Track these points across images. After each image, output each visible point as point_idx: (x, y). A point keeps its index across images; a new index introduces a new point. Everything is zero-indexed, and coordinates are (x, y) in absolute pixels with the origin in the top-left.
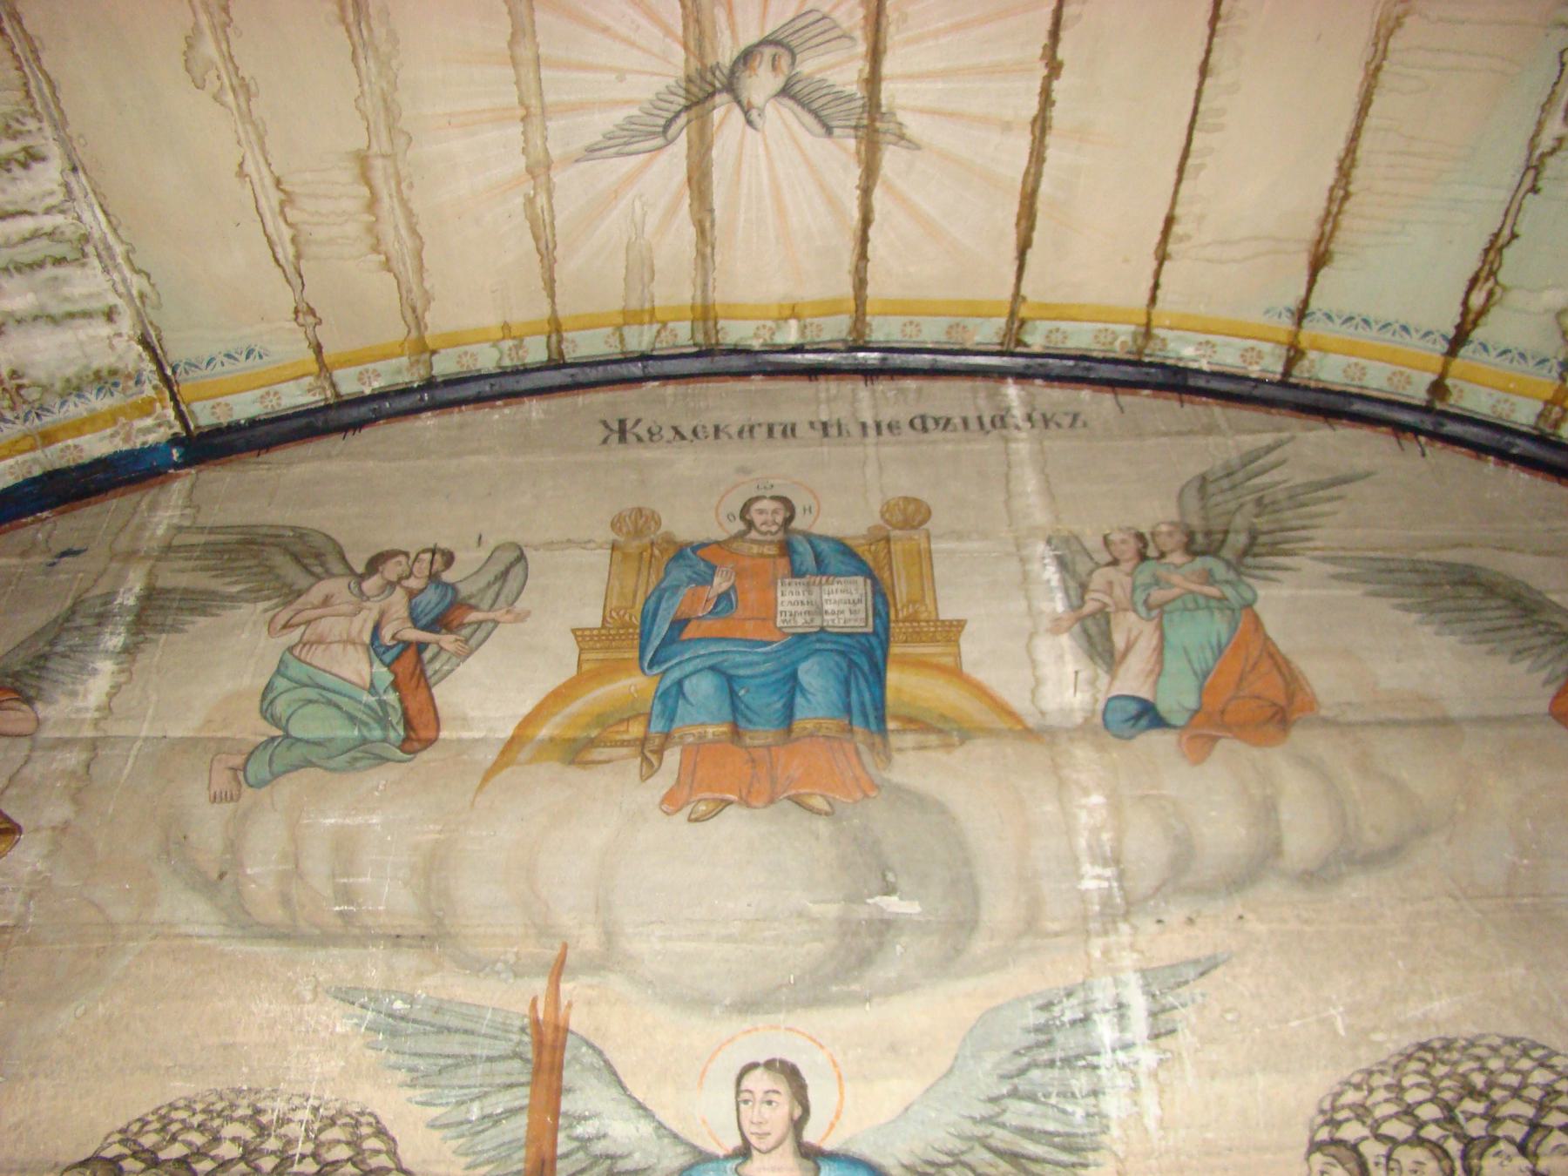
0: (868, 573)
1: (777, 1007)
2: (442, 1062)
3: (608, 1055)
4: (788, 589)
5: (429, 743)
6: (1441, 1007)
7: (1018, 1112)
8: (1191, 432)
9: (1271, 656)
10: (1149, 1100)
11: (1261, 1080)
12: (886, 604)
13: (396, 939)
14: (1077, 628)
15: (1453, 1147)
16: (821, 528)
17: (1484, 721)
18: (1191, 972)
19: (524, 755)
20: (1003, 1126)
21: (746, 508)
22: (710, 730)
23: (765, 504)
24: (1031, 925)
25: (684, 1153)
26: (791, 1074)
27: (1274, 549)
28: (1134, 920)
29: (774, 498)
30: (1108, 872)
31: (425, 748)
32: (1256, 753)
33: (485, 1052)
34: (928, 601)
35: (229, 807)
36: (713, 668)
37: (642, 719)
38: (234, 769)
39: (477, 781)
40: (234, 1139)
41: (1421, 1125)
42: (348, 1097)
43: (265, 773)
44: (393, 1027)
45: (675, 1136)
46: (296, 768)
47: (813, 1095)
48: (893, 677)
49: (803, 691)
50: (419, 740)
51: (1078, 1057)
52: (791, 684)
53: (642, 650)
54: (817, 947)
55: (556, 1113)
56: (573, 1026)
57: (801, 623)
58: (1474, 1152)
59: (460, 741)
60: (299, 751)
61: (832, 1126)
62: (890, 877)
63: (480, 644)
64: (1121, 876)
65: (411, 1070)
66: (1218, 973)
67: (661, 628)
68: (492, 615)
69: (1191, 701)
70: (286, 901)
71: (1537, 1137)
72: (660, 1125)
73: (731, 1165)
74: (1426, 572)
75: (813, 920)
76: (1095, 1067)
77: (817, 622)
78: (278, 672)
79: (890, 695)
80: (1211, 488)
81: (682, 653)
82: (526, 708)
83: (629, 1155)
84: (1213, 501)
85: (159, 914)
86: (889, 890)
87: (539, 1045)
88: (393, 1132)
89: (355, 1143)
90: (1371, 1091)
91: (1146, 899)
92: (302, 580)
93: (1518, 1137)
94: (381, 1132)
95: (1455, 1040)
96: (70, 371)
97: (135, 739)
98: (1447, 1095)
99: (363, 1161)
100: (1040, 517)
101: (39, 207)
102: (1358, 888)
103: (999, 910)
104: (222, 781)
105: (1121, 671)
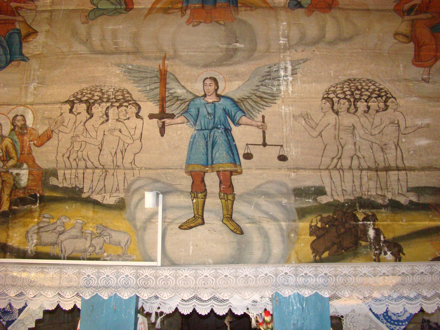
2: (140, 78)
3: (176, 76)
5: (131, 9)
6: (354, 72)
10: (290, 89)
11: (314, 84)
13: (128, 53)
15: (352, 100)
17: (378, 10)
19: (154, 11)
20: (259, 91)
22: (197, 6)
24: (268, 50)
28: (291, 50)
31: (130, 10)
32: (323, 15)
33: (150, 76)
35: (86, 25)
37: (181, 3)
38: (86, 16)
39: (143, 18)
40: (97, 96)
41: (346, 95)
42: (121, 86)
43: (94, 17)
44: (129, 71)
45: (191, 93)
46: (101, 15)
47: (219, 84)
50: (129, 8)
51: (276, 78)
55: (165, 88)
56: (168, 70)
58: (356, 101)
59: (139, 8)
60: (101, 12)
61: (223, 91)
64: (288, 41)
65: (134, 80)
66: (307, 62)
70: (102, 45)
71: (370, 99)
72: (187, 90)
75: (220, 48)
76: (279, 80)
83: (181, 96)
86: (237, 42)
88: (131, 93)
89: (123, 95)
90: (337, 88)
91: (294, 45)
93: (366, 99)
94: (128, 93)
97: (61, 10)
98: (353, 90)
99: (125, 99)
102: (341, 46)
103: (261, 47)
104: (84, 19)
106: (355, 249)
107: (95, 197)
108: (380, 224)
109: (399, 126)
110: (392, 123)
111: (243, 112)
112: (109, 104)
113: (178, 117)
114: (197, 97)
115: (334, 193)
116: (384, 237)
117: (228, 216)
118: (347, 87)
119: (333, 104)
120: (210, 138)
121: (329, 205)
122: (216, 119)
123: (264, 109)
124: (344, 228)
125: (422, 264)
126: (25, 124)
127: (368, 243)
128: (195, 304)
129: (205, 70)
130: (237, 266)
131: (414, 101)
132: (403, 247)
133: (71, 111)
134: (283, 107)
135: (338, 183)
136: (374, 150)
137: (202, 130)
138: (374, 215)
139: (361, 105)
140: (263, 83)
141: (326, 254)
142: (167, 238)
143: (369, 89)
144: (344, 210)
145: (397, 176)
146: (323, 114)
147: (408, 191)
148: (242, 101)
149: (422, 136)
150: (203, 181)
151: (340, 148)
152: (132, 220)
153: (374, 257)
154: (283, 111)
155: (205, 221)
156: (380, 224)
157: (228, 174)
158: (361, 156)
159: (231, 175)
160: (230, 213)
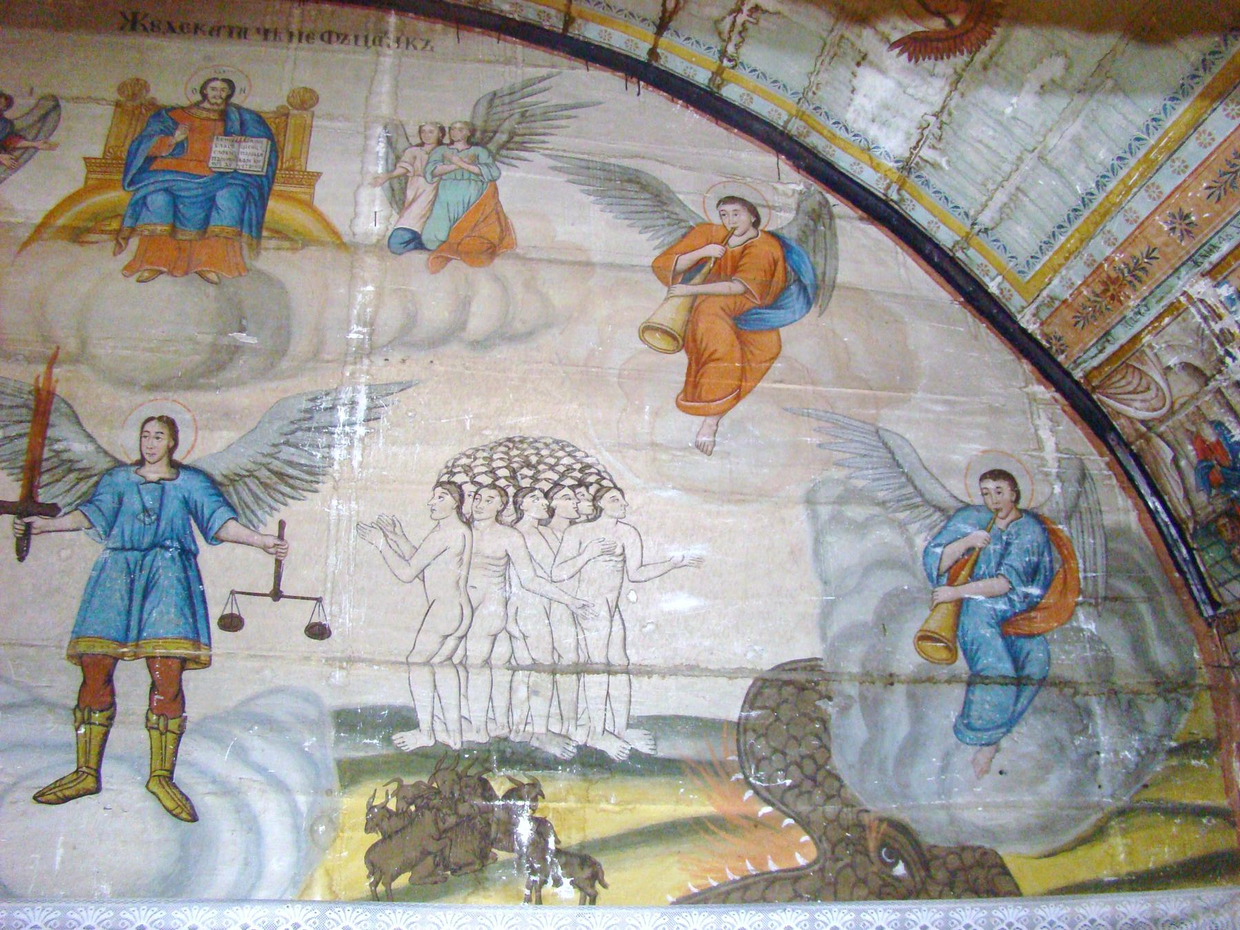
0: (270, 136)
1: (169, 389)
4: (219, 143)
7: (288, 453)
8: (498, 62)
9: (497, 213)
12: (277, 157)
14: (387, 184)
16: (246, 105)
21: (204, 87)
22: (159, 228)
23: (218, 84)
24: (316, 355)
25: (982, 670)
26: (171, 424)
27: (522, 147)
29: (224, 80)
30: (365, 330)
32: (470, 270)
33: (9, 404)
34: (303, 160)
39: (15, 248)
41: (498, 479)
47: (181, 436)
48: (272, 204)
49: (218, 209)
52: (210, 204)
53: (126, 173)
54: (197, 358)
55: (44, 438)
57: (223, 166)
59: (9, 223)
61: (189, 452)
62: (244, 322)
63: (26, 161)
64: (371, 334)
66: (410, 390)
67: (139, 162)
68: (35, 144)
69: (442, 236)
72: (99, 447)
73: (133, 469)
74: (609, 171)
77: (233, 166)
79: (268, 215)
80: (497, 102)
81: (148, 178)
82: (51, 206)
84: (494, 110)
86: (242, 330)
87: (38, 401)
90: (475, 459)
95: (525, 438)
98: (515, 466)
100: (385, 110)
103: (300, 345)
105: (406, 214)
108: (547, 808)
109: (624, 561)
110: (608, 552)
111: (234, 510)
113: (66, 514)
114: (120, 464)
115: (438, 726)
116: (557, 842)
117: (165, 773)
118: (501, 459)
119: (461, 500)
120: (141, 571)
122: (163, 524)
123: (285, 505)
124: (456, 813)
127: (515, 855)
129: (152, 397)
132: (604, 867)
134: (335, 502)
137: (123, 549)
138: (534, 785)
139: (534, 507)
141: (403, 880)
143: (557, 464)
146: (433, 524)
147: (629, 726)
148: (232, 481)
149: (681, 588)
150: (109, 680)
151: (467, 612)
153: (527, 892)
154: (334, 512)
155: (104, 785)
156: (547, 808)
157: (176, 665)
160: (168, 766)
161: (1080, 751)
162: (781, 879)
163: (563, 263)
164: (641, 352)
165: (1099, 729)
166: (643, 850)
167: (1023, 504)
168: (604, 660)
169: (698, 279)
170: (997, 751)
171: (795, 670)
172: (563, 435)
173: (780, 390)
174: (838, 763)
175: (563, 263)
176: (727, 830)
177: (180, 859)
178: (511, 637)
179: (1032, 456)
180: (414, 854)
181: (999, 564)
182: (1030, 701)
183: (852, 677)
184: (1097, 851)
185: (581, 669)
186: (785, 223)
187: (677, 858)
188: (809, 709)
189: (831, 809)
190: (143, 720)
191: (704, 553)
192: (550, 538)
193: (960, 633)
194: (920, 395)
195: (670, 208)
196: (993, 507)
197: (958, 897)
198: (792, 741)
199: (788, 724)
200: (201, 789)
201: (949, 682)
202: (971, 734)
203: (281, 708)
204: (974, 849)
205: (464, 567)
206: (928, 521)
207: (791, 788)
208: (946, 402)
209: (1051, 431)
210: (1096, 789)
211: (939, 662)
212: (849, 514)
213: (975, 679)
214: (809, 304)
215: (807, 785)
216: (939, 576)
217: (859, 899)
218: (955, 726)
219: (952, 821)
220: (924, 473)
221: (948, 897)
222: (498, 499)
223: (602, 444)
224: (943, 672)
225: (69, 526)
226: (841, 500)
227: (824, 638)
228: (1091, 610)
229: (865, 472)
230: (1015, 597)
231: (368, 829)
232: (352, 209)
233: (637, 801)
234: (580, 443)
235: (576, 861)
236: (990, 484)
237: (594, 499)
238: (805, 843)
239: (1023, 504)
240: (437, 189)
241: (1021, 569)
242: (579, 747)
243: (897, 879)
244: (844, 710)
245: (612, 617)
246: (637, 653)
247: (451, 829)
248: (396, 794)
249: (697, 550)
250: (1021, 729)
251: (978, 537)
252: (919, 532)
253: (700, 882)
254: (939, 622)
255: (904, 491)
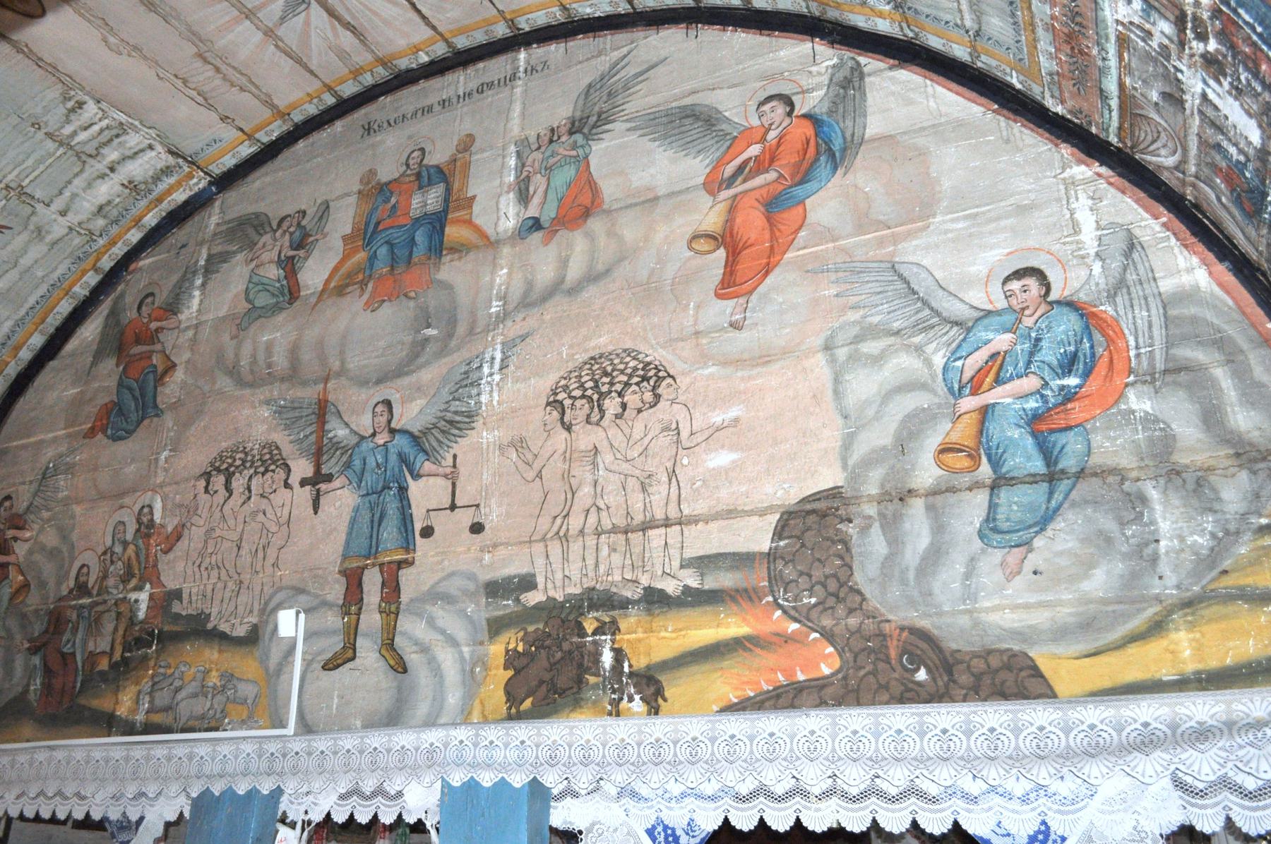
5: (298, 298)
7: (456, 406)
10: (496, 397)
18: (518, 341)
20: (449, 411)
25: (1008, 472)
36: (386, 242)
41: (586, 390)
48: (448, 230)
49: (416, 244)
52: (412, 242)
53: (364, 239)
60: (259, 312)
67: (372, 226)
78: (250, 282)
80: (592, 91)
85: (217, 386)
87: (320, 408)
89: (270, 453)
92: (256, 238)
94: (277, 448)
96: (151, 173)
98: (597, 377)
101: (96, 119)
106: (578, 693)
107: (224, 627)
108: (624, 639)
109: (679, 434)
110: (666, 429)
111: (427, 453)
112: (252, 471)
114: (363, 438)
115: (550, 585)
116: (630, 666)
118: (587, 374)
119: (563, 413)
121: (538, 607)
124: (561, 650)
125: (523, 726)
126: (152, 520)
127: (601, 679)
128: (914, 807)
130: (389, 731)
131: (711, 375)
132: (664, 684)
133: (206, 490)
134: (485, 434)
135: (557, 565)
136: (629, 490)
137: (368, 494)
138: (614, 622)
139: (612, 405)
140: (456, 395)
141: (527, 704)
142: (306, 686)
143: (626, 368)
144: (563, 616)
145: (664, 537)
146: (546, 434)
147: (682, 567)
148: (424, 433)
149: (723, 447)
151: (569, 496)
152: (264, 661)
153: (609, 707)
154: (485, 440)
156: (624, 639)
157: (394, 567)
158: (602, 506)
159: (399, 568)
160: (391, 636)
161: (1132, 541)
162: (808, 688)
163: (636, 205)
164: (689, 259)
165: (1158, 515)
166: (694, 668)
167: (1053, 296)
168: (664, 517)
169: (738, 182)
170: (1030, 550)
171: (819, 499)
172: (629, 345)
173: (803, 255)
174: (859, 578)
175: (636, 205)
176: (762, 648)
177: (397, 700)
178: (599, 509)
179: (1064, 244)
180: (534, 683)
181: (1029, 363)
182: (1067, 495)
183: (871, 499)
184: (1154, 648)
185: (645, 527)
186: (817, 101)
187: (719, 674)
188: (831, 532)
189: (853, 621)
190: (377, 606)
191: (740, 413)
192: (624, 427)
193: (984, 440)
194: (939, 218)
195: (718, 127)
196: (1018, 308)
197: (985, 700)
198: (817, 564)
199: (812, 549)
200: (408, 650)
201: (970, 489)
202: (998, 537)
203: (453, 587)
204: (1002, 652)
205: (568, 463)
206: (945, 338)
207: (815, 605)
208: (966, 218)
209: (1091, 210)
210: (1157, 581)
211: (961, 471)
212: (865, 350)
213: (1000, 482)
214: (835, 168)
215: (831, 601)
216: (961, 388)
217: (881, 703)
218: (980, 531)
219: (976, 624)
220: (941, 292)
221: (974, 700)
222: (587, 405)
223: (658, 343)
224: (966, 479)
225: (339, 486)
226: (858, 339)
227: (845, 466)
228: (1145, 388)
229: (881, 308)
230: (1048, 392)
231: (506, 668)
232: (495, 216)
233: (688, 628)
234: (642, 348)
235: (644, 681)
236: (1015, 285)
237: (654, 388)
238: (830, 655)
239: (1053, 296)
240: (549, 179)
241: (1055, 363)
242: (645, 589)
243: (919, 684)
244: (865, 530)
245: (670, 480)
246: (689, 506)
247: (558, 662)
248: (522, 640)
249: (734, 412)
250: (1059, 524)
251: (1002, 341)
252: (936, 350)
253: (739, 693)
254: (963, 433)
255: (920, 315)
